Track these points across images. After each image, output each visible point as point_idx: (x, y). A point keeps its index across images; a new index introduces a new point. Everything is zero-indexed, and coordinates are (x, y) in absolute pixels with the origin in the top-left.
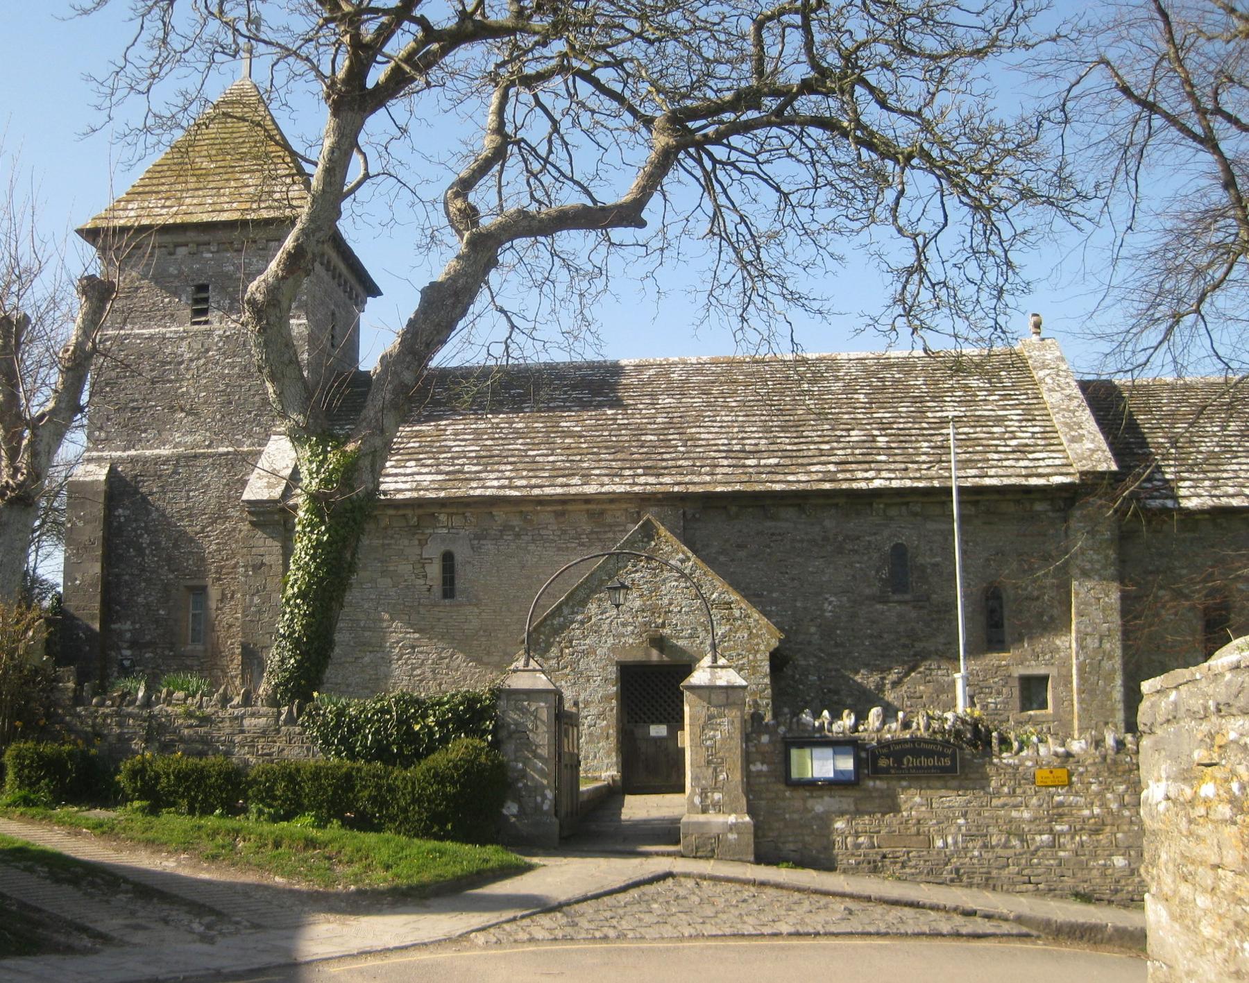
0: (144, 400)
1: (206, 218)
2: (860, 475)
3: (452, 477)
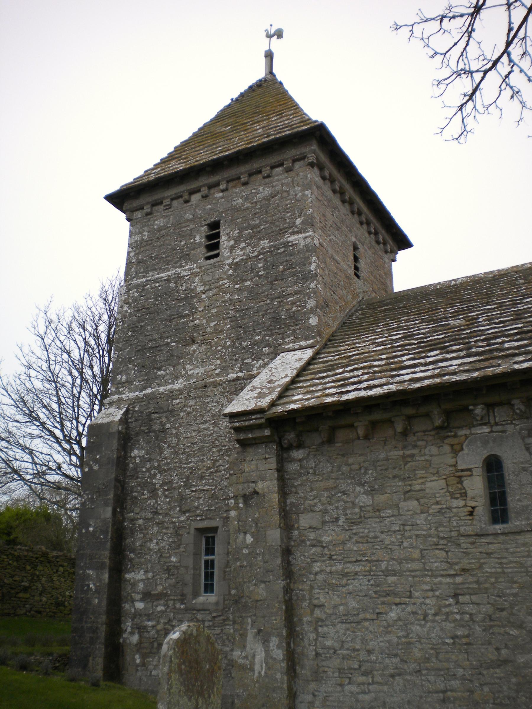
0: (161, 338)
3: (486, 357)
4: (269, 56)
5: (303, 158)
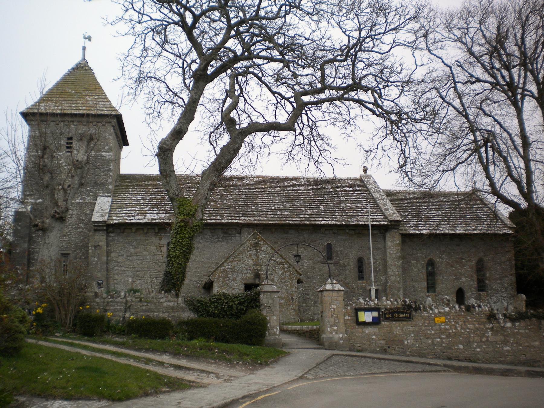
1: (73, 112)
2: (317, 219)
4: (84, 49)
5: (110, 123)
